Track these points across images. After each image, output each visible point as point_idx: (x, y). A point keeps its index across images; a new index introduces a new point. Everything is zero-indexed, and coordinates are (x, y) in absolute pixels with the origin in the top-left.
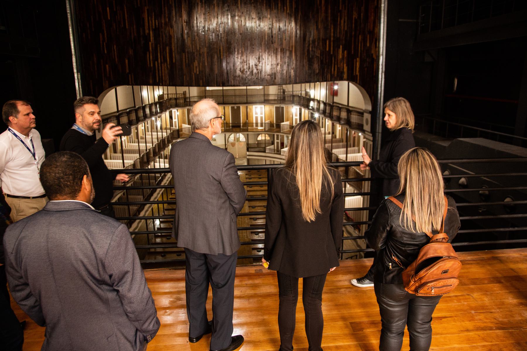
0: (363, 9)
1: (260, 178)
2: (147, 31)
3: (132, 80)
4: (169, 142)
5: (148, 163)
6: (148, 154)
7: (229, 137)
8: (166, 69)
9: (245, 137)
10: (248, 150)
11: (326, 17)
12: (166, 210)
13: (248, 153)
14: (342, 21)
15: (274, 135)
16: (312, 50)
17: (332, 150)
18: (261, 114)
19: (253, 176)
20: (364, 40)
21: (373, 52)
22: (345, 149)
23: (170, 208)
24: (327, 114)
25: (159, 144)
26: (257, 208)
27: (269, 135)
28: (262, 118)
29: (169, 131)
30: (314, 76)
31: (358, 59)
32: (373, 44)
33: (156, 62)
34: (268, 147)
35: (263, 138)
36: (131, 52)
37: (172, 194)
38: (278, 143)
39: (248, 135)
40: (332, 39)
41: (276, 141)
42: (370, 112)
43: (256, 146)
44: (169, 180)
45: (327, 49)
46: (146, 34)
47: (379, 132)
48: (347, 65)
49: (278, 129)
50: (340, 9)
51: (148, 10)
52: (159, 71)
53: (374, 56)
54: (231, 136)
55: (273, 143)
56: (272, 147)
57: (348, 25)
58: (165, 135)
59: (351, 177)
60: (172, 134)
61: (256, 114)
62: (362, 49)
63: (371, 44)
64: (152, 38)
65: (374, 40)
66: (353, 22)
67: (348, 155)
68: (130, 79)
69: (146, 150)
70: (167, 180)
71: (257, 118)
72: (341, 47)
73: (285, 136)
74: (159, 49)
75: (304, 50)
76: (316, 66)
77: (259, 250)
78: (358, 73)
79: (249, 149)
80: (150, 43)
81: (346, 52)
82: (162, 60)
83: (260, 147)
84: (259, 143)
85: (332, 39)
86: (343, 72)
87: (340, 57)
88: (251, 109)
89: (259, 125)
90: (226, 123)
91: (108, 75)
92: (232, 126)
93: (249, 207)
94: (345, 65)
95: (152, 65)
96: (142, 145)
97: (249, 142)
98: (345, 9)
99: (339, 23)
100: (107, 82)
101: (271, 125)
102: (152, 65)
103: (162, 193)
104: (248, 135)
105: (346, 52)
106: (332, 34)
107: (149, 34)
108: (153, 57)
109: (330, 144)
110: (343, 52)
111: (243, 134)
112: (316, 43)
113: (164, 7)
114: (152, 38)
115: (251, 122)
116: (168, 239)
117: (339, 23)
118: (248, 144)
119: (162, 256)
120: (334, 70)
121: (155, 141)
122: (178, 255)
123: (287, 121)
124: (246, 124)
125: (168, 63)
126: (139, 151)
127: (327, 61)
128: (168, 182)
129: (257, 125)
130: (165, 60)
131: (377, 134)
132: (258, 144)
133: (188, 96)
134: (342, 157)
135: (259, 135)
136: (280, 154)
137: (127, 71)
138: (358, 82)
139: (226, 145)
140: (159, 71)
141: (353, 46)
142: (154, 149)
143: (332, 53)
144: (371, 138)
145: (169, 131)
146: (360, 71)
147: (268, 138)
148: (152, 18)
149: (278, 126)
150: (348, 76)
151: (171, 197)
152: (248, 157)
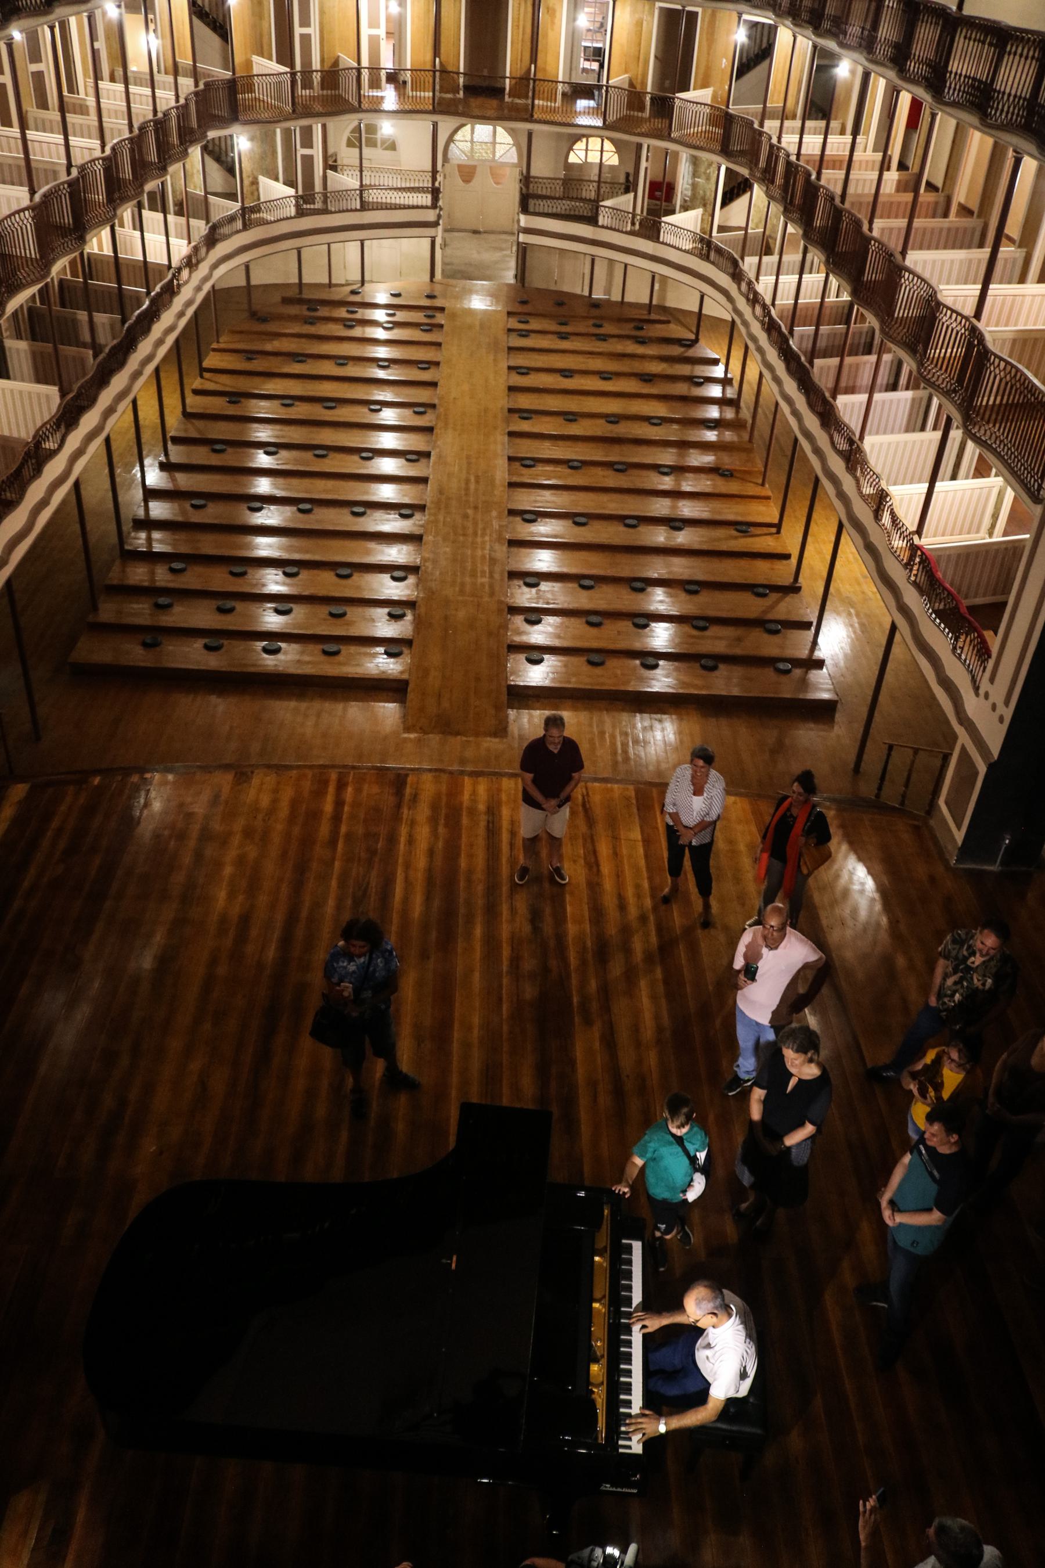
1: (563, 336)
4: (187, 137)
5: (79, 231)
6: (77, 189)
7: (450, 139)
9: (517, 144)
10: (525, 209)
12: (176, 440)
13: (524, 220)
15: (639, 146)
17: (904, 253)
19: (535, 324)
23: (194, 434)
24: (911, 66)
25: (137, 142)
26: (540, 468)
29: (187, 84)
34: (607, 203)
35: (594, 158)
37: (203, 370)
39: (530, 135)
43: (559, 191)
44: (190, 312)
49: (659, 123)
54: (459, 136)
56: (624, 201)
58: (166, 98)
59: (988, 398)
60: (204, 97)
69: (69, 165)
70: (181, 314)
73: (685, 155)
77: (535, 656)
79: (532, 202)
83: (573, 197)
84: (572, 179)
90: (444, 71)
92: (466, 88)
93: (510, 459)
96: (46, 144)
97: (534, 172)
101: (634, 96)
103: (157, 370)
104: (530, 135)
109: (903, 223)
111: (512, 132)
116: (173, 571)
118: (526, 179)
119: (145, 645)
121: (118, 130)
122: (221, 610)
123: (705, 85)
124: (526, 83)
126: (28, 173)
128: (183, 322)
132: (567, 182)
134: (958, 295)
135: (578, 138)
139: (434, 172)
142: (110, 164)
145: (187, 84)
147: (612, 158)
149: (663, 106)
151: (197, 383)
152: (522, 238)
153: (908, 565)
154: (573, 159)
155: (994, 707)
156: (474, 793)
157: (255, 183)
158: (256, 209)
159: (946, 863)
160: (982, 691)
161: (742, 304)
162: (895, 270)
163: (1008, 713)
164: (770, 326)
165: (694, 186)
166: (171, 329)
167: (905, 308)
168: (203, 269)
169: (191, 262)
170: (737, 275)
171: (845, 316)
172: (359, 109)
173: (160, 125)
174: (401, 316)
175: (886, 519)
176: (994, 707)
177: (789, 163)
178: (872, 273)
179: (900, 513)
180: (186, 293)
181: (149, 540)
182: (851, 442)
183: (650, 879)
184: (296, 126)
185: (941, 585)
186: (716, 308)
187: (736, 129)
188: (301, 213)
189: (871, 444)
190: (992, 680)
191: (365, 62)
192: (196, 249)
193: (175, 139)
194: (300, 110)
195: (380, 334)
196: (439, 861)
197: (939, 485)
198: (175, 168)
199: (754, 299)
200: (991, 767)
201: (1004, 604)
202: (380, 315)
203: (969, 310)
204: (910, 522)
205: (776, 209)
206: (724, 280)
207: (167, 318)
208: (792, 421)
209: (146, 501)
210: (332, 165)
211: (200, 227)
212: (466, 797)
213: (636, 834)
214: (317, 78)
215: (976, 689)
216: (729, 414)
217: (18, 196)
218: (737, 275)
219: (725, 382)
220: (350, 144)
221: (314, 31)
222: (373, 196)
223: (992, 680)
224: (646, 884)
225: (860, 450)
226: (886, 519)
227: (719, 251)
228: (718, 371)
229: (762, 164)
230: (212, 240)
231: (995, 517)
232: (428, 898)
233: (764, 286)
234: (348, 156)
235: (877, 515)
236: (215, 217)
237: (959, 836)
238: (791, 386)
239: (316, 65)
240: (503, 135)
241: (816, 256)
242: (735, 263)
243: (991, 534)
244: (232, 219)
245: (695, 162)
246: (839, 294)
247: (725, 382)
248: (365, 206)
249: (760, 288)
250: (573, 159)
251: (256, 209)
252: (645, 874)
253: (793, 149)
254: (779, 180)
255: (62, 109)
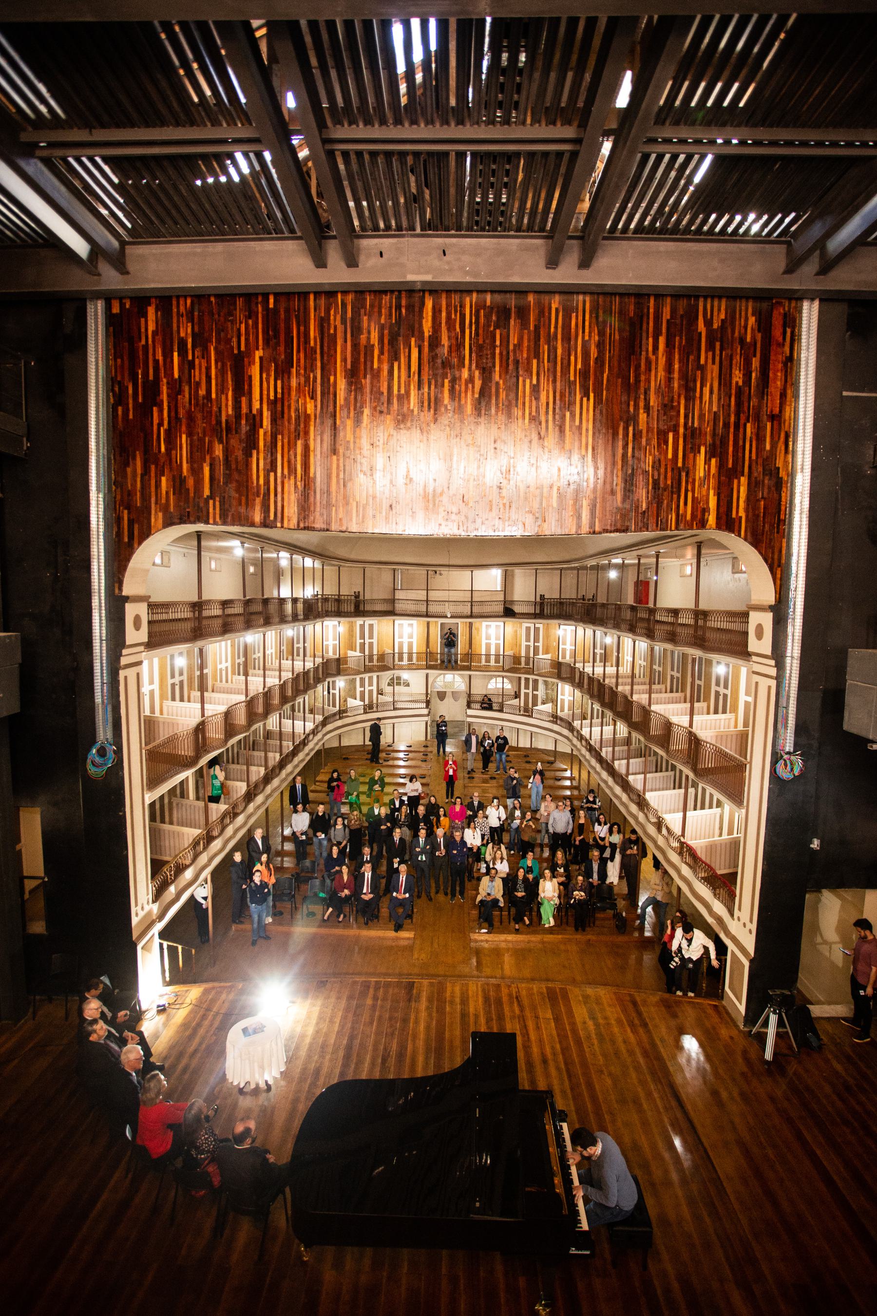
0: (756, 362)
2: (256, 405)
3: (215, 514)
4: (318, 680)
7: (434, 681)
8: (293, 489)
10: (469, 707)
11: (669, 380)
14: (706, 390)
15: (520, 678)
16: (633, 456)
17: (650, 705)
18: (497, 638)
20: (759, 438)
21: (780, 463)
22: (688, 705)
27: (511, 680)
28: (497, 646)
30: (636, 516)
31: (742, 479)
32: (781, 446)
33: (272, 474)
36: (218, 451)
38: (526, 695)
40: (681, 430)
41: (523, 691)
42: (771, 608)
45: (670, 456)
46: (254, 412)
47: (792, 657)
48: (719, 495)
50: (702, 362)
51: (261, 358)
52: (276, 495)
53: (782, 474)
55: (517, 696)
56: (515, 702)
57: (719, 399)
61: (488, 638)
62: (754, 457)
63: (774, 445)
64: (266, 422)
65: (783, 435)
66: (733, 392)
67: (695, 718)
68: (211, 510)
70: (308, 754)
71: (488, 646)
72: (703, 449)
74: (279, 444)
75: (614, 456)
76: (642, 495)
78: (742, 513)
79: (472, 705)
80: (261, 431)
81: (713, 461)
82: (286, 472)
85: (681, 430)
86: (705, 510)
87: (700, 472)
88: (478, 629)
89: (493, 658)
91: (163, 501)
94: (712, 492)
95: (261, 482)
98: (714, 363)
99: (698, 395)
100: (160, 515)
102: (261, 482)
105: (713, 461)
106: (682, 421)
107: (260, 411)
108: (265, 464)
110: (707, 462)
112: (644, 441)
113: (298, 351)
114: (266, 422)
115: (478, 652)
117: (698, 395)
120: (686, 504)
121: (287, 675)
125: (299, 476)
127: (669, 482)
129: (488, 661)
130: (292, 470)
131: (788, 660)
133: (361, 598)
136: (531, 716)
137: (207, 492)
138: (586, 686)
139: (427, 694)
140: (276, 495)
141: (731, 449)
143: (680, 464)
144: (773, 672)
146: (747, 510)
147: (508, 686)
148: (268, 375)
150: (718, 518)
153: (681, 854)
154: (490, 686)
155: (744, 925)
156: (453, 992)
157: (346, 701)
158: (345, 711)
159: (737, 1026)
160: (735, 917)
161: (575, 741)
162: (646, 712)
163: (754, 927)
164: (591, 749)
165: (547, 694)
166: (303, 760)
167: (655, 729)
168: (319, 736)
169: (314, 732)
170: (571, 728)
171: (628, 741)
172: (394, 669)
173: (306, 673)
174: (411, 755)
175: (664, 831)
176: (744, 925)
177: (589, 678)
178: (636, 718)
179: (671, 827)
180: (311, 745)
181: (282, 861)
182: (639, 796)
183: (560, 1042)
184: (366, 676)
185: (701, 860)
186: (564, 747)
187: (563, 669)
188: (365, 712)
189: (649, 796)
190: (740, 909)
191: (396, 651)
192: (317, 726)
193: (312, 681)
194: (368, 670)
195: (401, 763)
196: (433, 1034)
197: (688, 814)
198: (311, 692)
199: (581, 738)
200: (752, 961)
201: (736, 873)
202: (401, 755)
203: (686, 724)
204: (677, 830)
205: (586, 697)
206: (566, 732)
207: (301, 756)
208: (607, 791)
209: (283, 842)
210: (380, 693)
211: (319, 718)
212: (448, 994)
213: (549, 1015)
214: (375, 658)
215: (732, 915)
216: (576, 793)
217: (243, 698)
218: (571, 728)
219: (571, 779)
220: (389, 685)
221: (375, 641)
222: (399, 705)
223: (740, 909)
224: (558, 1046)
225: (645, 799)
226: (664, 831)
227: (561, 719)
228: (568, 774)
229: (577, 680)
230: (324, 723)
231: (721, 828)
232: (427, 1058)
233: (585, 732)
234: (388, 689)
235: (659, 829)
236: (326, 714)
237: (742, 1008)
238: (604, 775)
239: (375, 652)
240: (458, 679)
241: (609, 714)
242: (570, 724)
243: (721, 835)
244: (335, 714)
245: (546, 682)
246: (622, 729)
247: (571, 779)
248: (395, 709)
249: (583, 733)
250: (490, 686)
251: (345, 711)
252: (557, 1039)
253: (591, 673)
254: (586, 686)
255: (264, 670)
